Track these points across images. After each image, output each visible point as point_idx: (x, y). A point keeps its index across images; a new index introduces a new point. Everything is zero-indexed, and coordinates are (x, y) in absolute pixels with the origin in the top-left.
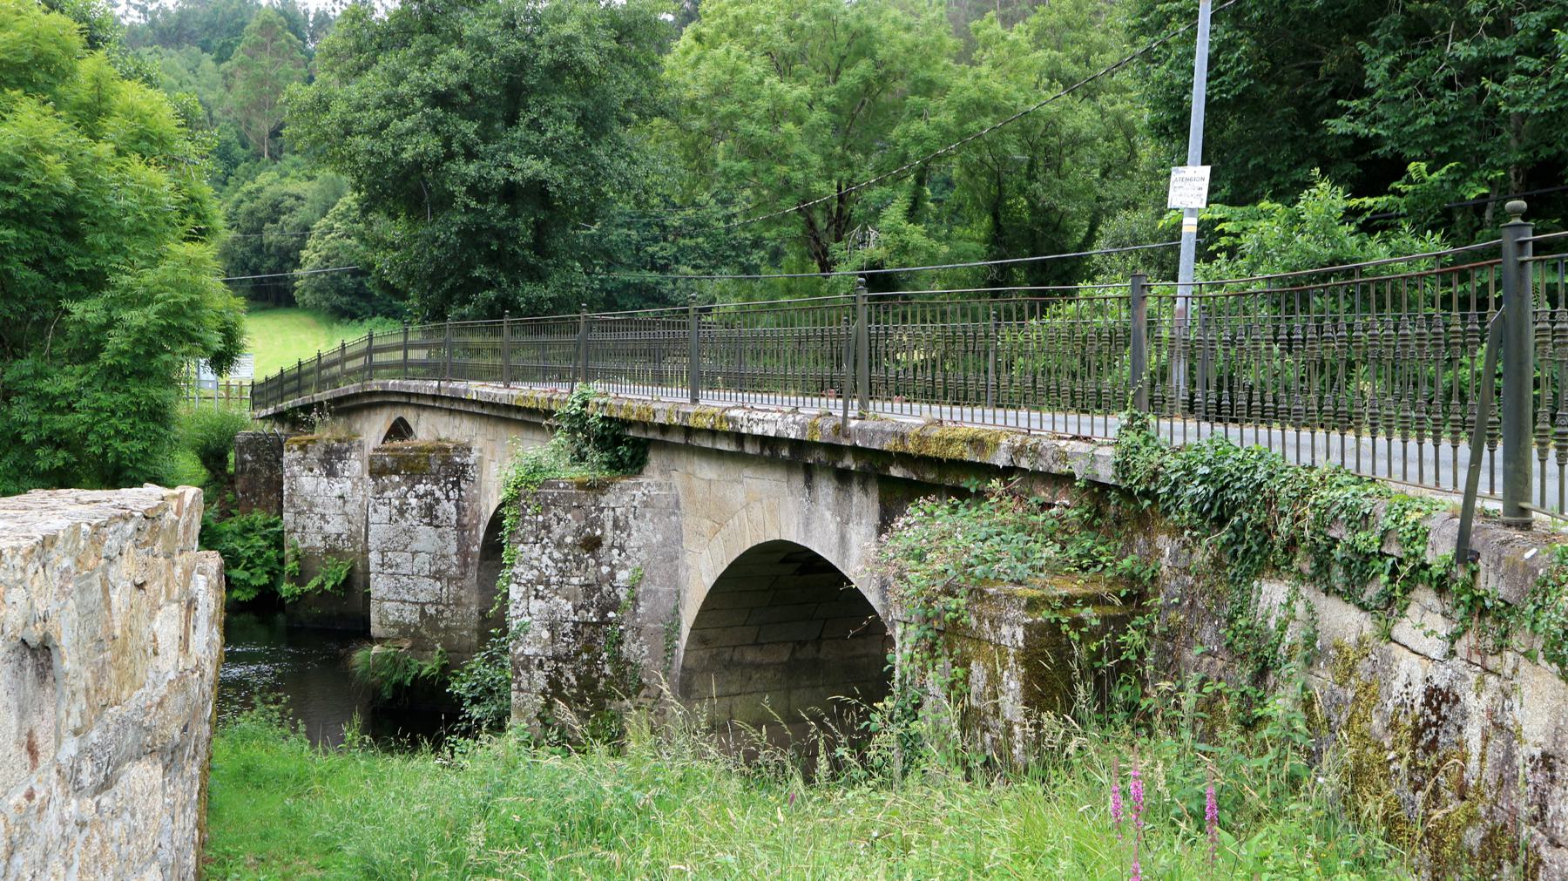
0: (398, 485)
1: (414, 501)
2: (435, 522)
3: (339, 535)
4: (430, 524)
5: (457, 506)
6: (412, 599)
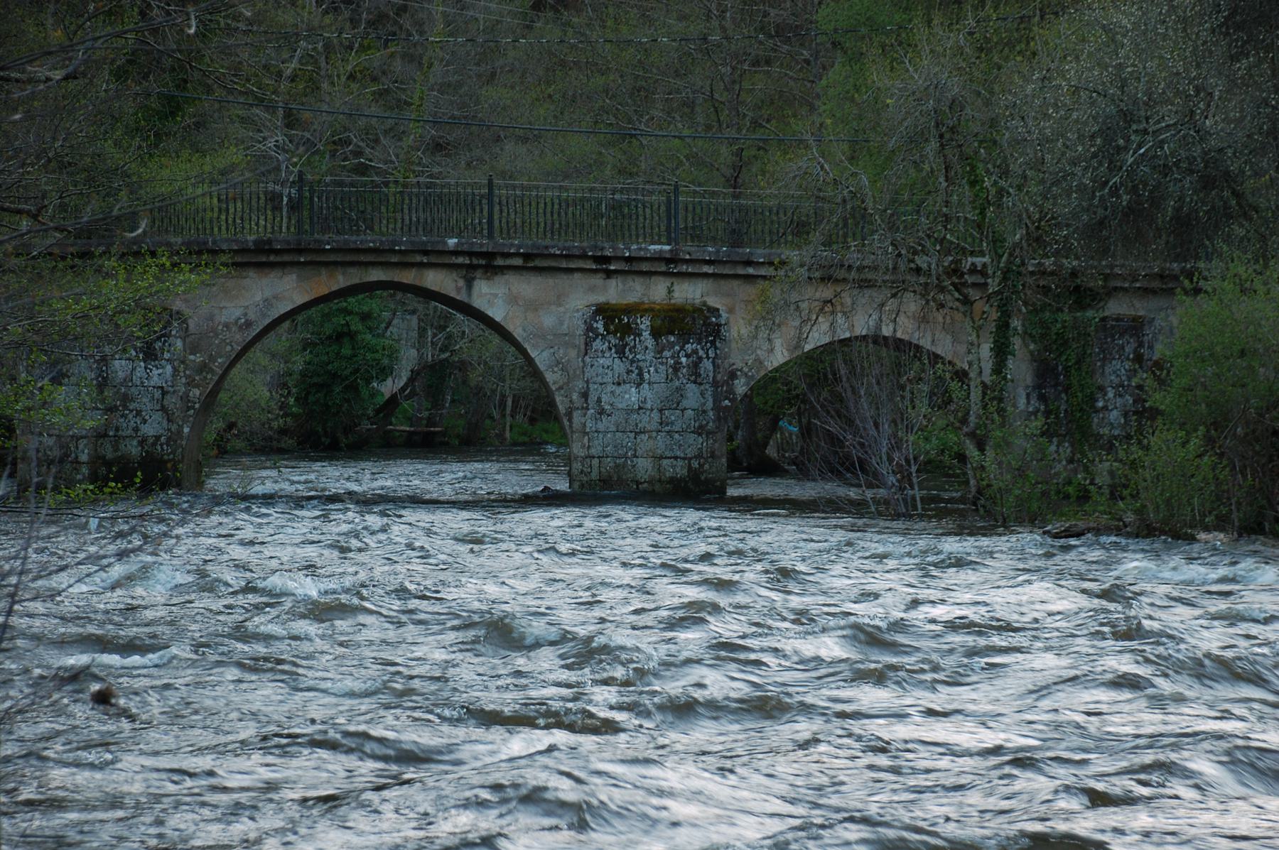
0: (672, 345)
1: (684, 360)
2: (699, 380)
3: (158, 438)
4: (695, 382)
5: (713, 363)
6: (682, 455)
